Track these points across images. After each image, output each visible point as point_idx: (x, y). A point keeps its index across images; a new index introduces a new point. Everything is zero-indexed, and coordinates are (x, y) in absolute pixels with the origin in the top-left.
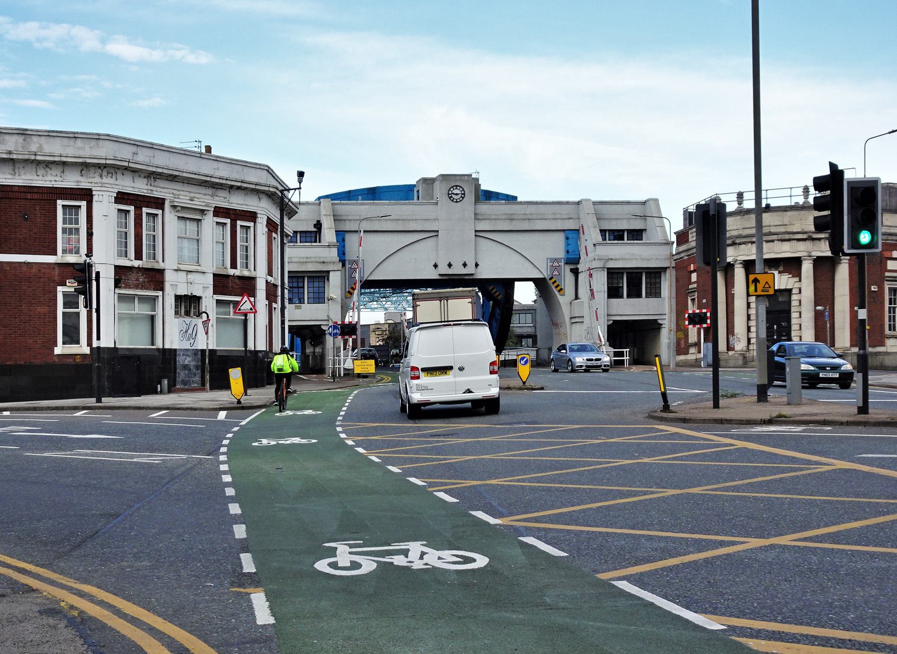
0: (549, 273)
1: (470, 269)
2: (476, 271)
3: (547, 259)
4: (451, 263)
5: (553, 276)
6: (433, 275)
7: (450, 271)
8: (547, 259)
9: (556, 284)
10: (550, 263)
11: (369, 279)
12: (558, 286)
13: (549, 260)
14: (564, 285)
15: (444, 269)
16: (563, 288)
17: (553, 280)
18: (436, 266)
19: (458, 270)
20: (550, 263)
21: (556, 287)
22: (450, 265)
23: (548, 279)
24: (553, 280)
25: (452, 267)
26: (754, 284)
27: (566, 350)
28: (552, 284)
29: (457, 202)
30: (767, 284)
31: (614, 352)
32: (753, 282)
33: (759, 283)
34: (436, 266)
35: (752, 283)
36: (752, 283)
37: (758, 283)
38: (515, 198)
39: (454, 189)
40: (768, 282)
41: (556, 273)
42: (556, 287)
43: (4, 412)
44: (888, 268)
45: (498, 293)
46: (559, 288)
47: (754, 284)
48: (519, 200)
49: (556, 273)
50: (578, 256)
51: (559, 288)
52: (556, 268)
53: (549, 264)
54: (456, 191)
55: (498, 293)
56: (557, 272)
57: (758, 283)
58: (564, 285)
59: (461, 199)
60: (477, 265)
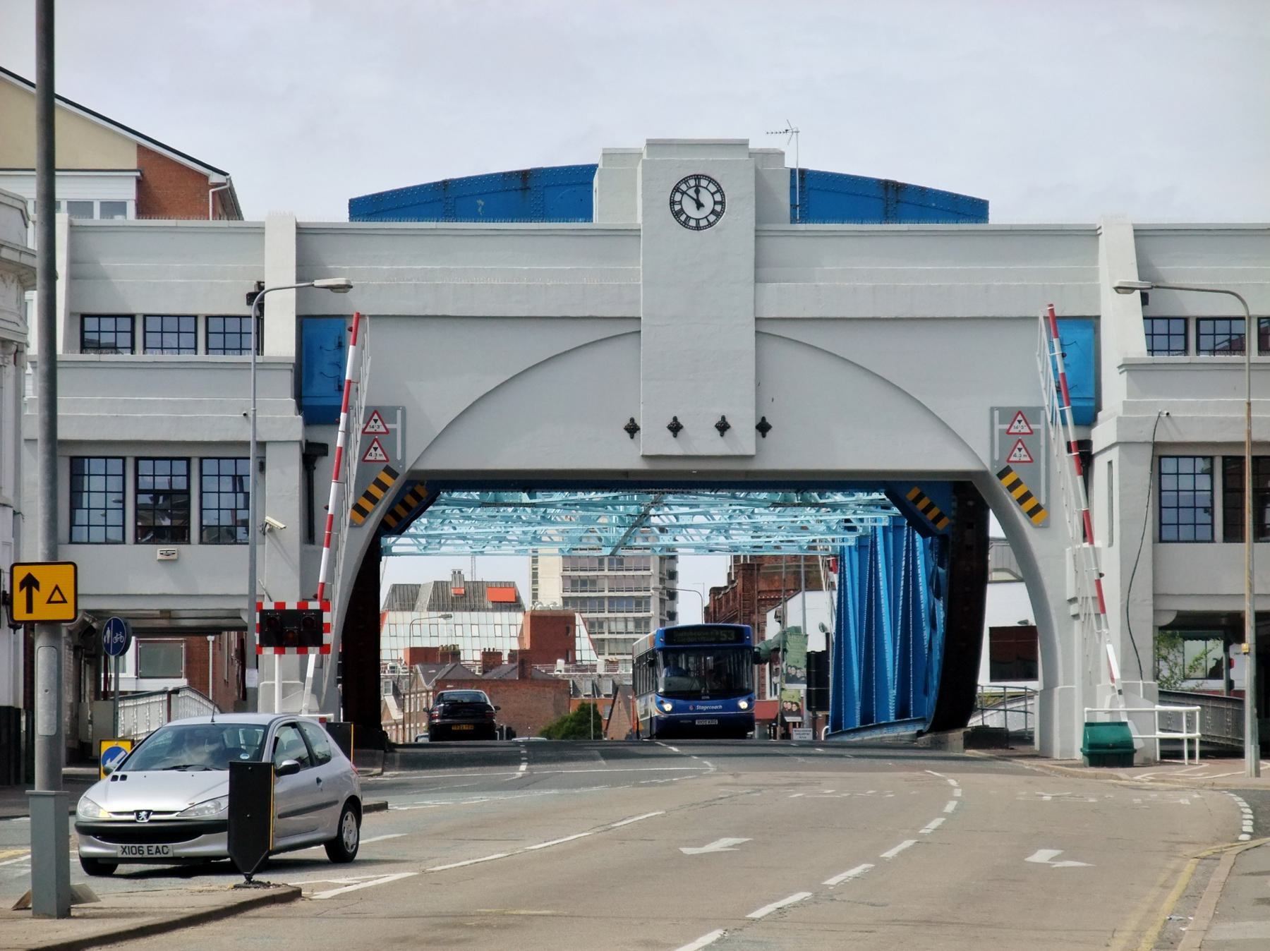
0: (997, 457)
1: (743, 440)
2: (758, 449)
3: (992, 410)
4: (680, 420)
5: (1011, 465)
6: (626, 457)
7: (672, 447)
8: (992, 410)
9: (1019, 492)
10: (1001, 422)
11: (413, 468)
12: (1026, 497)
13: (996, 413)
14: (1048, 498)
15: (656, 441)
16: (1043, 502)
17: (1009, 479)
18: (632, 429)
19: (711, 446)
20: (1001, 422)
21: (1022, 500)
22: (675, 428)
23: (994, 474)
24: (1009, 479)
25: (727, 433)
26: (25, 590)
27: (777, 723)
28: (1006, 493)
29: (698, 228)
30: (61, 599)
31: (1161, 714)
32: (22, 585)
33: (38, 588)
34: (632, 429)
35: (21, 588)
36: (21, 588)
37: (34, 590)
38: (974, 210)
39: (713, 194)
40: (60, 586)
41: (1021, 455)
42: (1022, 500)
43: (308, 676)
44: (139, 495)
45: (935, 512)
46: (1030, 504)
47: (25, 590)
48: (996, 217)
49: (1021, 455)
50: (1092, 404)
51: (1030, 504)
52: (1020, 440)
53: (998, 427)
54: (706, 198)
55: (935, 512)
56: (379, 451)
57: (34, 590)
58: (1048, 498)
59: (712, 218)
60: (763, 427)
